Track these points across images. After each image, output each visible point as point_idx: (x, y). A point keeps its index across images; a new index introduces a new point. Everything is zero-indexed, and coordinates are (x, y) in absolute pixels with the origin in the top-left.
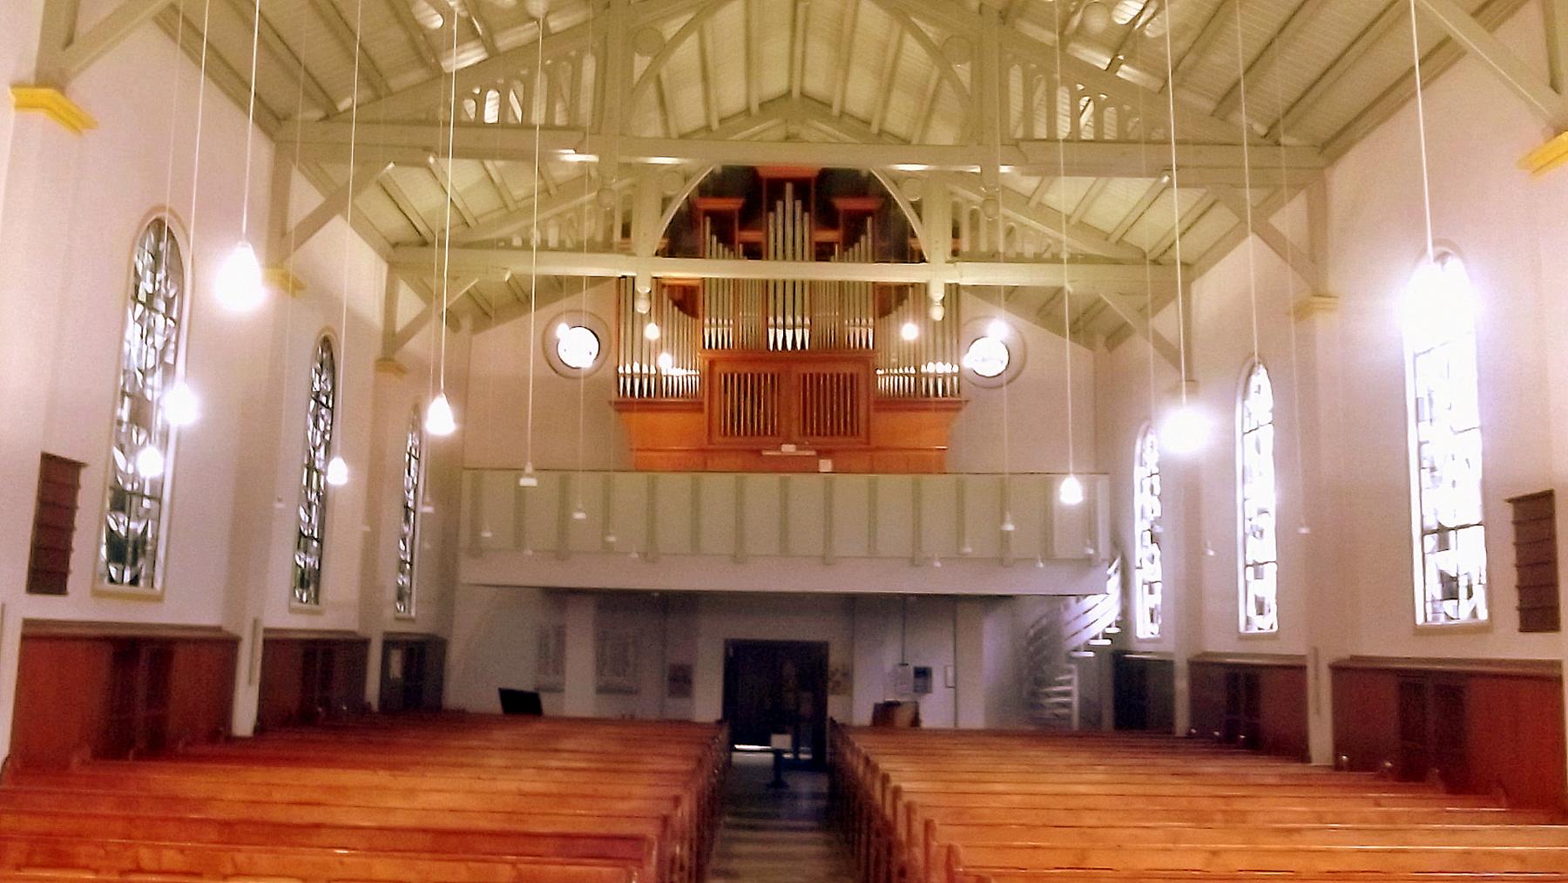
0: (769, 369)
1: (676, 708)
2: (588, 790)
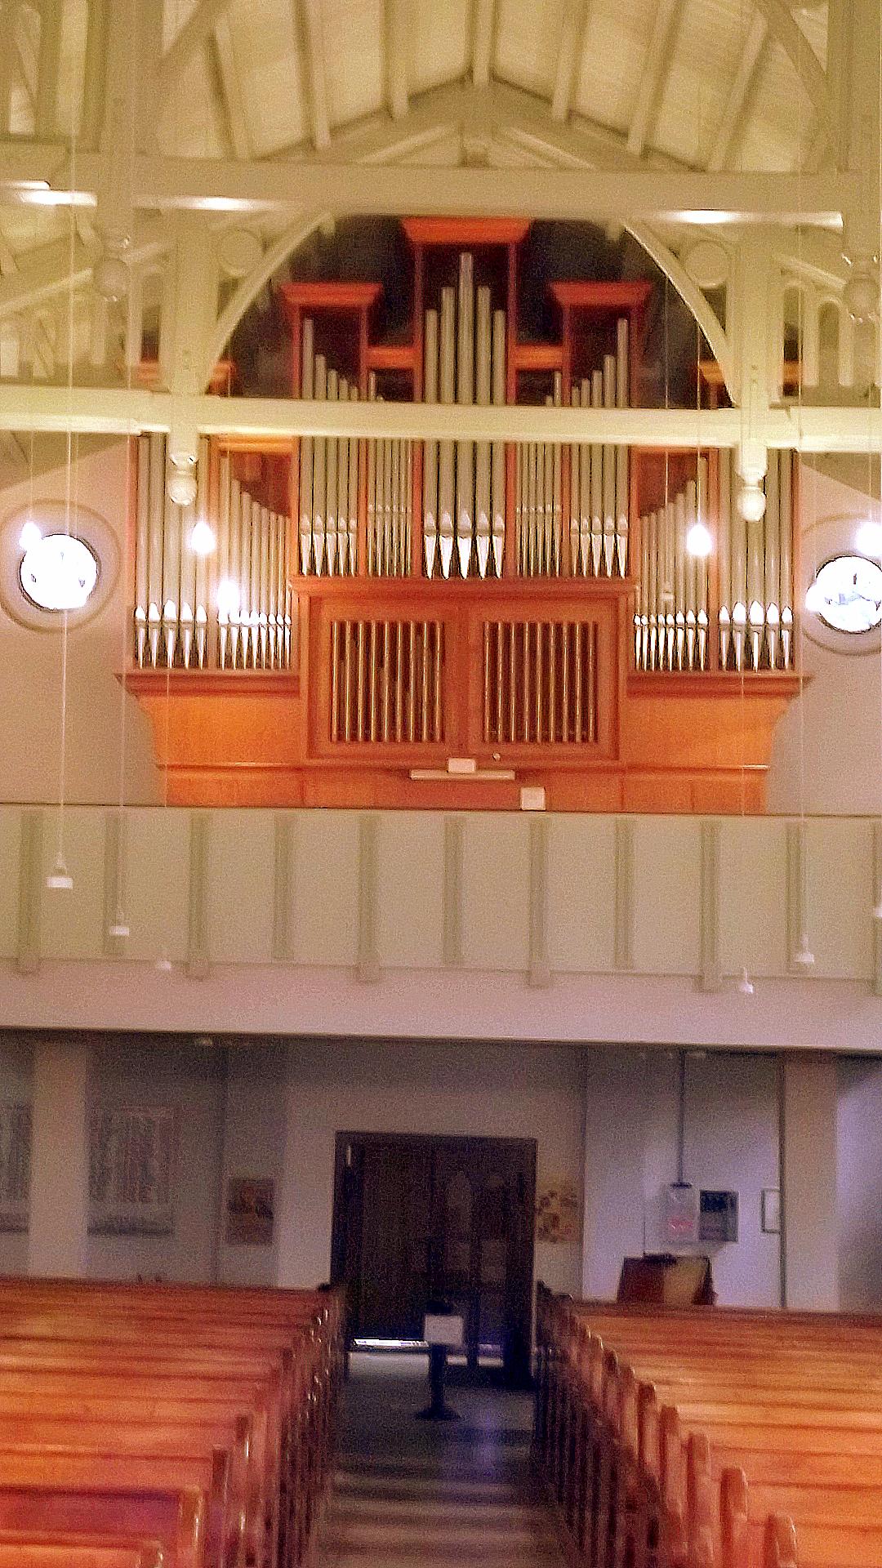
0: (428, 614)
1: (243, 1264)
2: (74, 1407)
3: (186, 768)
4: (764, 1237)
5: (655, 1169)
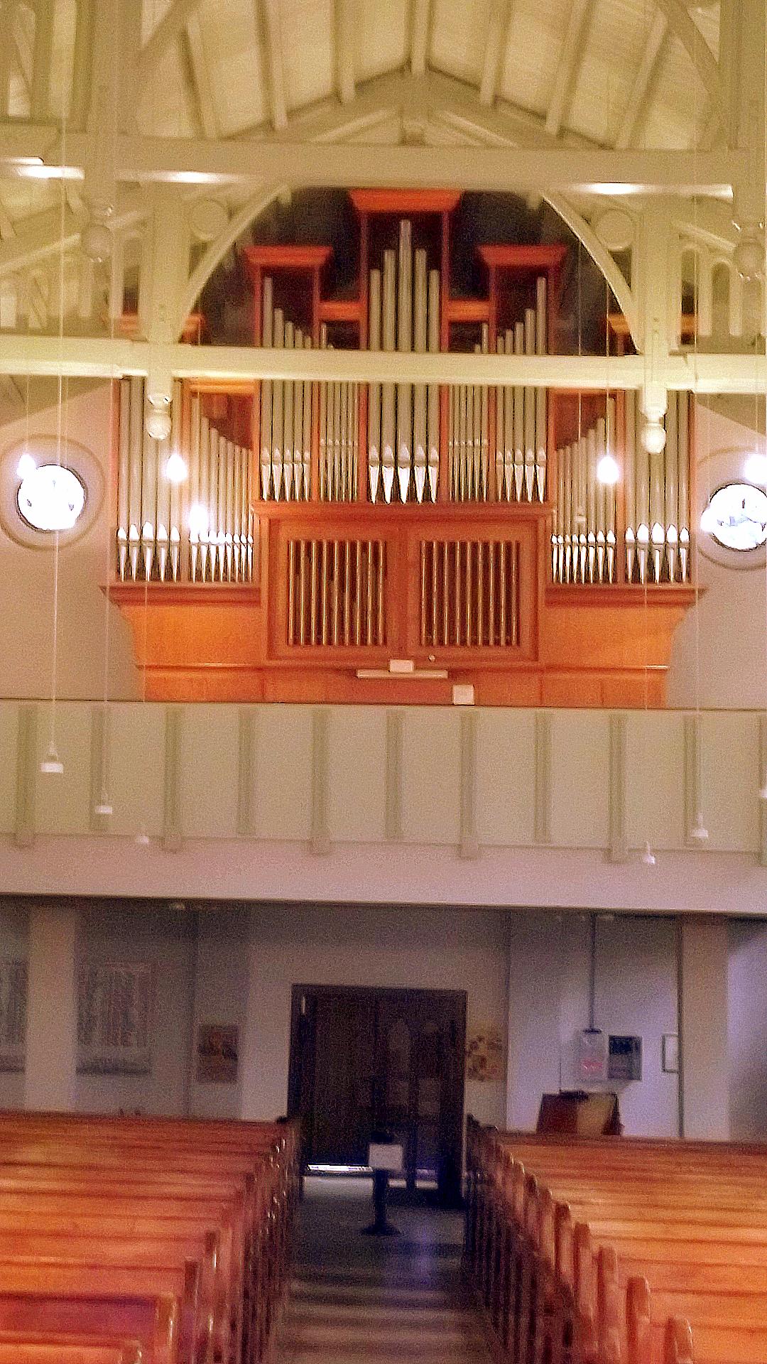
0: (372, 534)
1: (211, 1099)
2: (64, 1224)
3: (162, 668)
4: (665, 1076)
5: (570, 1017)
